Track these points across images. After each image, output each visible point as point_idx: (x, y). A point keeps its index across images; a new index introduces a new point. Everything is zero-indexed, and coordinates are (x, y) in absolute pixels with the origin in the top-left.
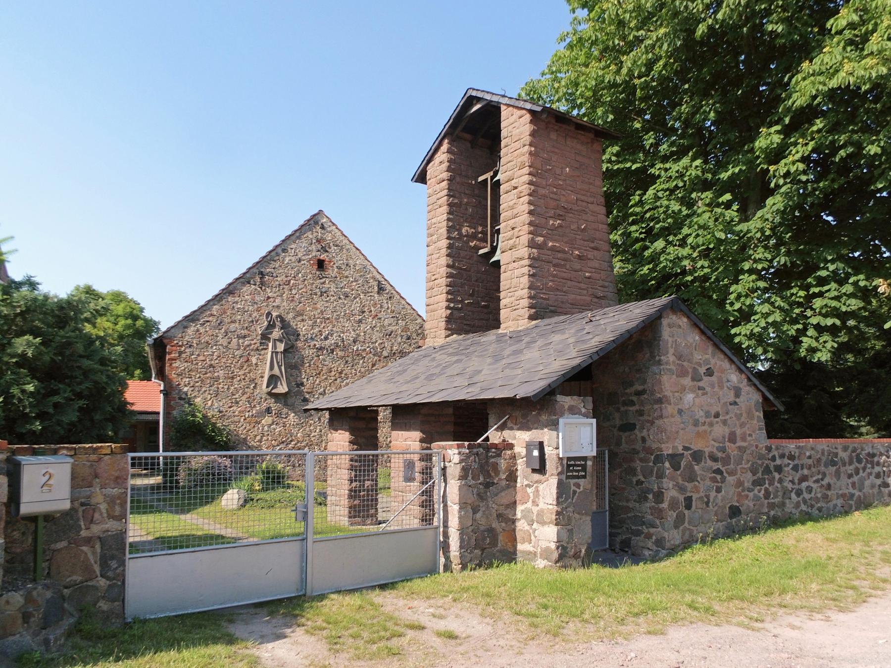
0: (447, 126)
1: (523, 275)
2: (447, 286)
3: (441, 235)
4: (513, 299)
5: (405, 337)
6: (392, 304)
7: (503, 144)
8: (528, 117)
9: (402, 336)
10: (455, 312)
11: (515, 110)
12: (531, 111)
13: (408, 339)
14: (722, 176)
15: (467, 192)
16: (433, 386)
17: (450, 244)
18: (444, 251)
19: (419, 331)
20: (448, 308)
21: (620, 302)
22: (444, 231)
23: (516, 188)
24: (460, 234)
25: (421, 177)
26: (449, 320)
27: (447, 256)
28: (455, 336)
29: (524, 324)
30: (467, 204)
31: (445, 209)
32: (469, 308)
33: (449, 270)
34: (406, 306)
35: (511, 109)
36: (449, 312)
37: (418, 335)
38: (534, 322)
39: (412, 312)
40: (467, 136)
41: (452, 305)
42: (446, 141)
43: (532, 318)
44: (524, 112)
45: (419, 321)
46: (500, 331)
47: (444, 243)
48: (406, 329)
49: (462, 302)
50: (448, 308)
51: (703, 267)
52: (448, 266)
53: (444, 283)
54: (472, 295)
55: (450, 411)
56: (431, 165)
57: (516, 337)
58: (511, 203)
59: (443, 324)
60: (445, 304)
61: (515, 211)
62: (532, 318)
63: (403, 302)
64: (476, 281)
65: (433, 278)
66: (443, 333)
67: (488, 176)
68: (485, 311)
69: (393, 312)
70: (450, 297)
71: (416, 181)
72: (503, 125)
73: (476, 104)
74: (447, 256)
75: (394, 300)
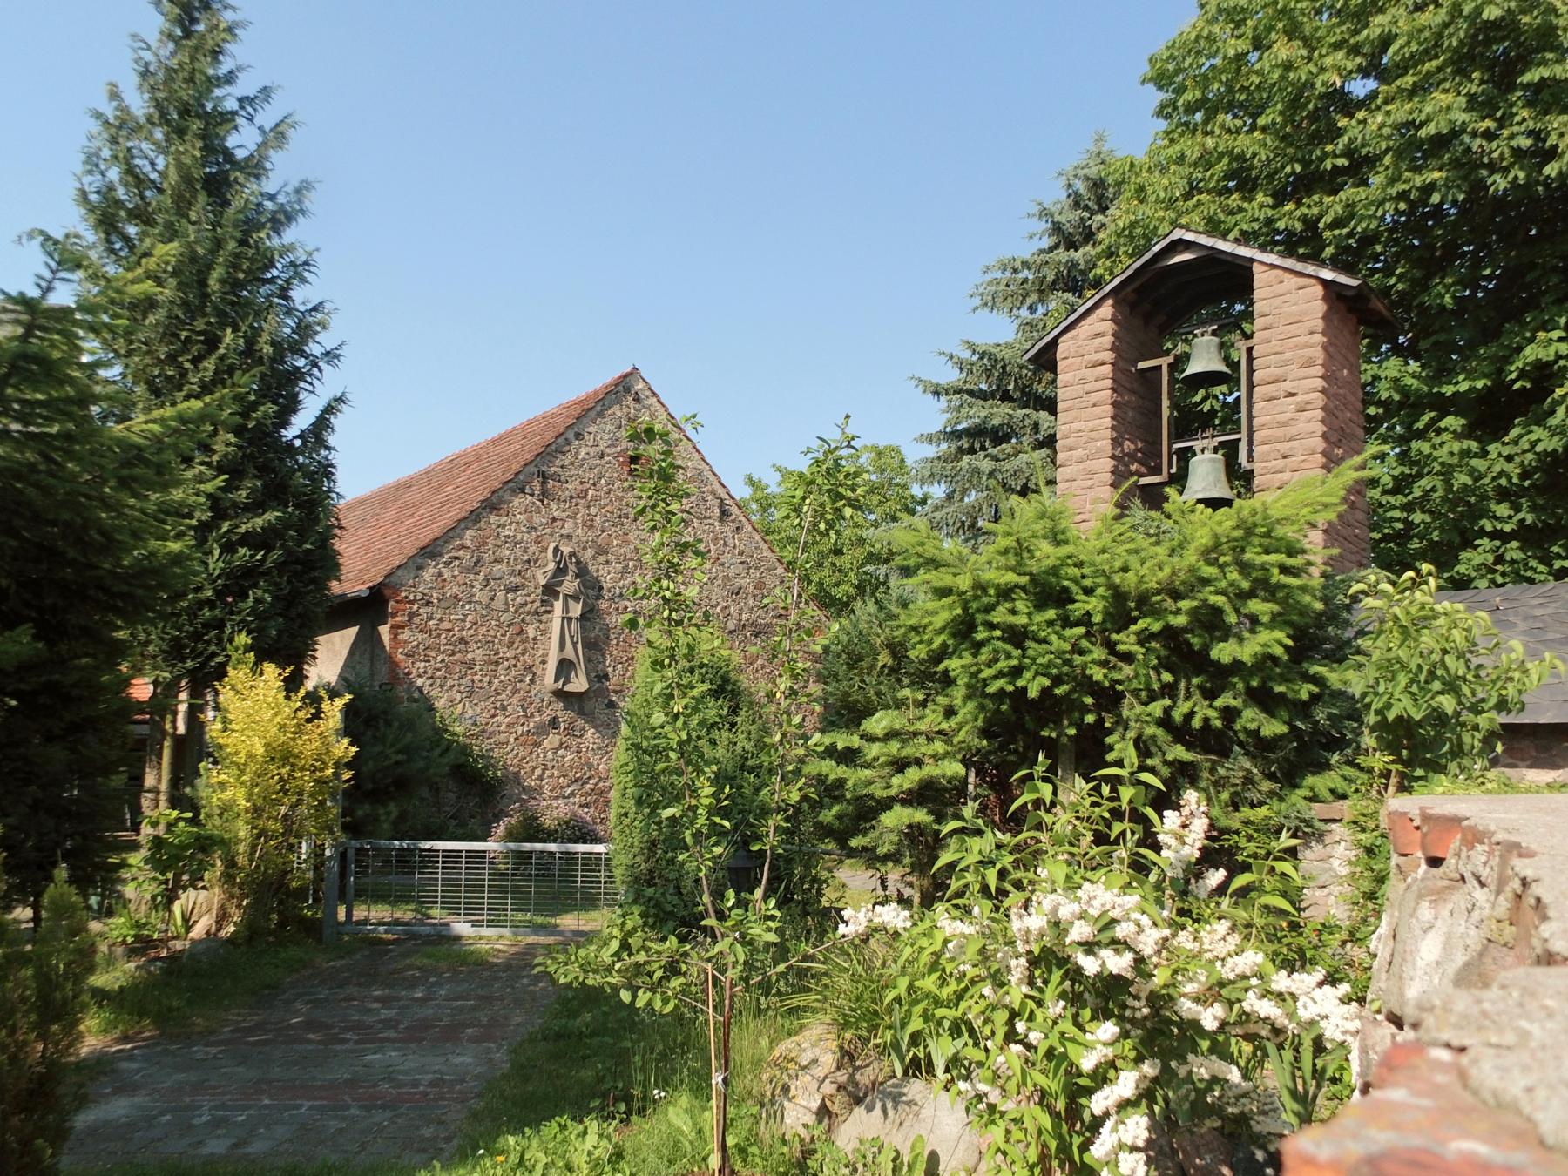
3: (1099, 450)
6: (740, 540)
8: (1319, 290)
22: (1106, 444)
31: (1108, 410)
35: (1279, 272)
42: (1110, 302)
56: (1073, 333)
58: (1283, 418)
61: (1292, 431)
69: (741, 553)
73: (1181, 252)
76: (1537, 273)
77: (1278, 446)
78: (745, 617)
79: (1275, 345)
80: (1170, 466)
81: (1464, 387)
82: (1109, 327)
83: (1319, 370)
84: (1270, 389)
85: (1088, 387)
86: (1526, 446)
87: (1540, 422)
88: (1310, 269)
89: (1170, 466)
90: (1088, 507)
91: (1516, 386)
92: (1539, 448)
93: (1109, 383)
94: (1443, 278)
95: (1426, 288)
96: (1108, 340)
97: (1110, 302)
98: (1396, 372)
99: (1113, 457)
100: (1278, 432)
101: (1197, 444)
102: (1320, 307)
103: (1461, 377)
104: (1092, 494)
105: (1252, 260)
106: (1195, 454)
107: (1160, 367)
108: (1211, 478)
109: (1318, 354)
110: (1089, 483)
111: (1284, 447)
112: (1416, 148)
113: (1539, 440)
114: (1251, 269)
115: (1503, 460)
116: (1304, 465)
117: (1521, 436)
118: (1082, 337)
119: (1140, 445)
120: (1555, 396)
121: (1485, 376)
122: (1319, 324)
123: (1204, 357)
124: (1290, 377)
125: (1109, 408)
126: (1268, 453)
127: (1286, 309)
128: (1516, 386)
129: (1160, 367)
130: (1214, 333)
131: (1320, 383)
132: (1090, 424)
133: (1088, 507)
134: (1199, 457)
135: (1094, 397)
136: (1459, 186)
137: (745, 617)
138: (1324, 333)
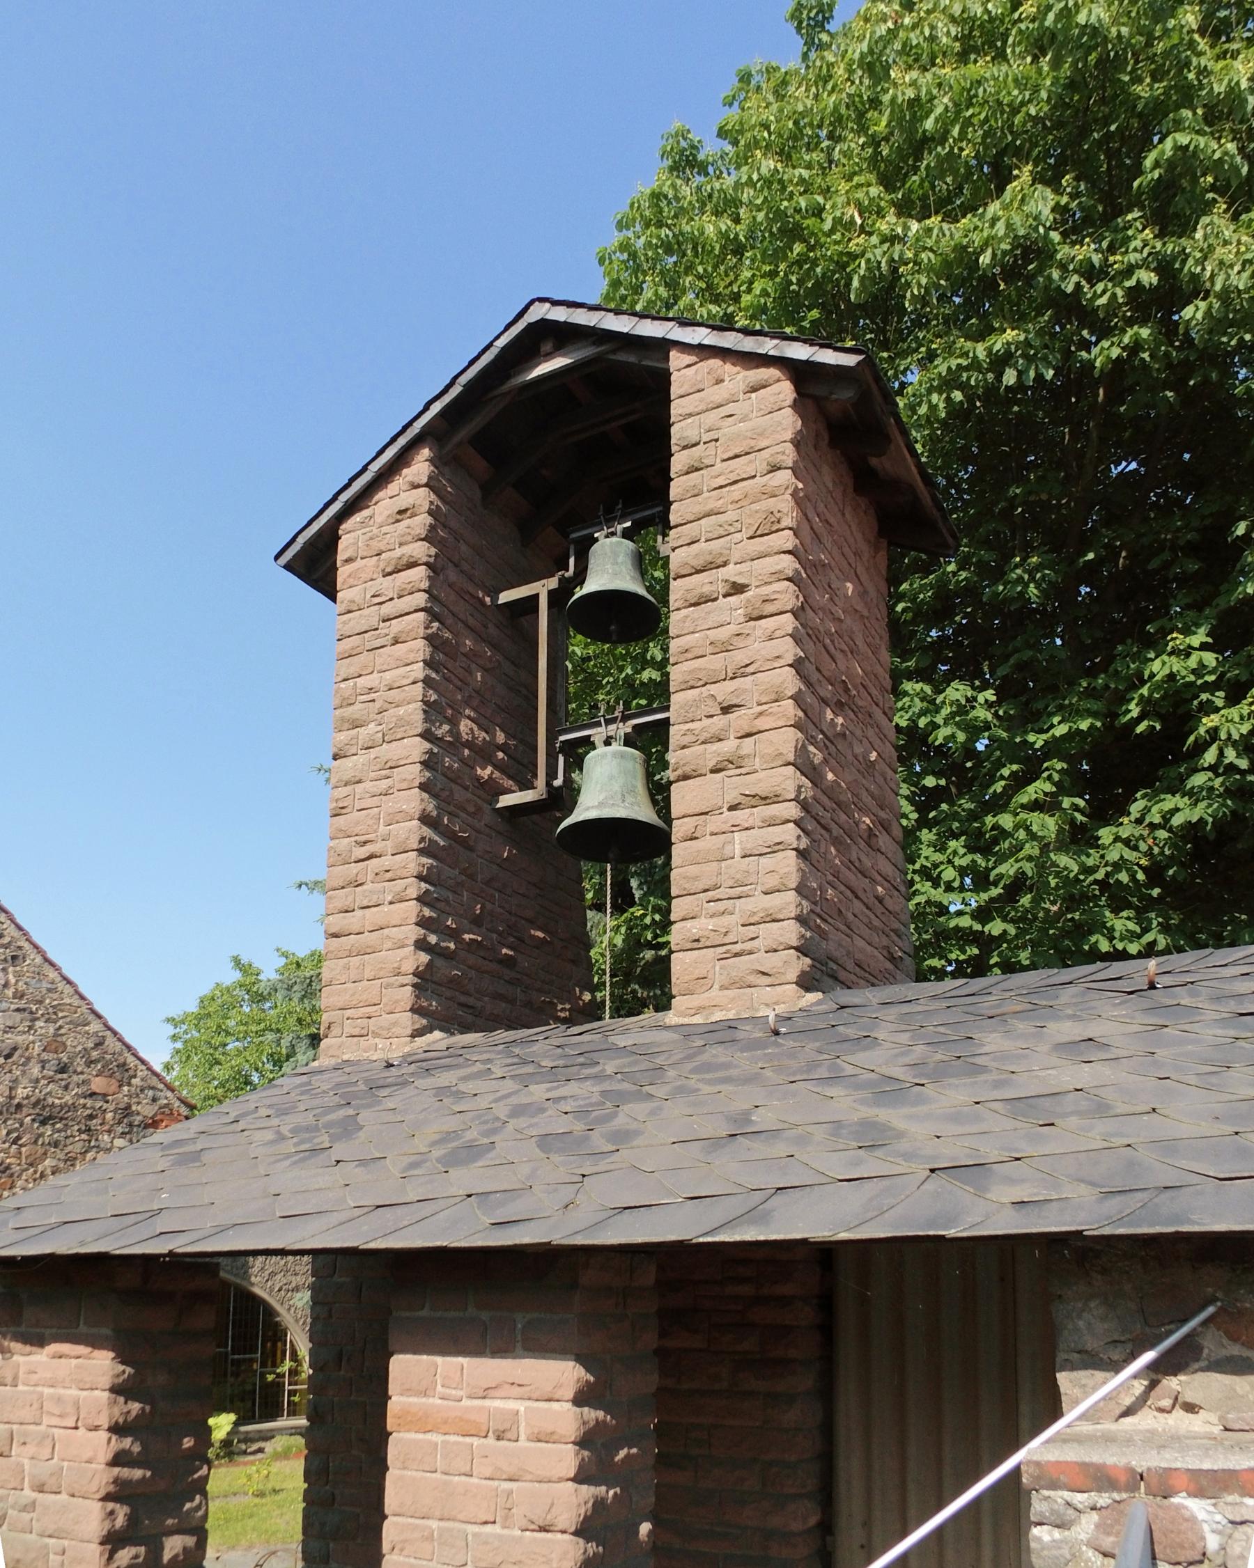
0: (436, 408)
1: (776, 848)
2: (420, 878)
3: (401, 722)
4: (726, 920)
5: (52, 1065)
6: (18, 975)
7: (678, 462)
8: (785, 390)
9: (43, 1063)
10: (440, 962)
11: (729, 368)
12: (800, 372)
13: (63, 1069)
14: (1031, 738)
15: (471, 621)
16: (738, 1170)
17: (430, 752)
18: (415, 773)
19: (95, 1054)
20: (421, 945)
21: (916, 981)
22: (413, 713)
23: (737, 589)
24: (455, 732)
25: (315, 563)
26: (424, 981)
27: (423, 787)
28: (437, 1034)
29: (783, 997)
30: (472, 656)
31: (418, 649)
32: (472, 959)
33: (427, 832)
34: (61, 985)
35: (715, 363)
36: (424, 958)
37: (89, 1063)
38: (813, 997)
39: (76, 1001)
40: (480, 465)
41: (433, 939)
42: (426, 452)
43: (806, 983)
44: (773, 372)
45: (95, 1027)
46: (671, 1018)
47: (417, 748)
48: (54, 1044)
49: (454, 934)
50: (421, 945)
51: (562, 1010)
52: (425, 819)
53: (413, 868)
54: (477, 922)
55: (648, 1276)
56: (357, 518)
57: (382, 1081)
58: (722, 634)
59: (406, 995)
60: (415, 932)
61: (739, 657)
62: (806, 983)
63: (53, 975)
64: (488, 883)
65: (362, 852)
66: (408, 1022)
67: (542, 588)
68: (508, 973)
69: (19, 995)
70: (427, 912)
71: (288, 567)
72: (676, 409)
73: (548, 356)
74: (423, 787)
75: (24, 967)
76: (1166, 556)
77: (713, 689)
78: (21, 1092)
79: (710, 501)
80: (551, 774)
81: (1061, 730)
82: (423, 498)
83: (786, 540)
84: (701, 584)
85: (387, 609)
86: (1157, 819)
87: (1175, 788)
88: (769, 346)
89: (551, 774)
90: (382, 829)
91: (1140, 729)
92: (1177, 821)
93: (421, 599)
94: (1024, 560)
95: (998, 574)
96: (421, 522)
97: (426, 452)
98: (961, 707)
99: (426, 735)
100: (715, 663)
101: (598, 734)
102: (788, 423)
103: (1056, 720)
104: (389, 804)
105: (664, 346)
106: (593, 746)
107: (536, 596)
108: (616, 787)
109: (785, 507)
110: (384, 784)
111: (724, 691)
112: (978, 292)
113: (1177, 810)
114: (663, 378)
115: (1124, 844)
116: (762, 723)
117: (1147, 810)
118: (378, 519)
119: (501, 737)
120: (1202, 730)
121: (1094, 715)
122: (789, 455)
123: (610, 567)
124: (735, 555)
125: (421, 643)
126: (696, 703)
127: (728, 429)
128: (1140, 729)
129: (536, 596)
130: (627, 534)
131: (788, 564)
132: (388, 676)
133: (382, 829)
134: (601, 749)
135: (396, 626)
136: (1045, 359)
137: (21, 1092)
138: (794, 470)
